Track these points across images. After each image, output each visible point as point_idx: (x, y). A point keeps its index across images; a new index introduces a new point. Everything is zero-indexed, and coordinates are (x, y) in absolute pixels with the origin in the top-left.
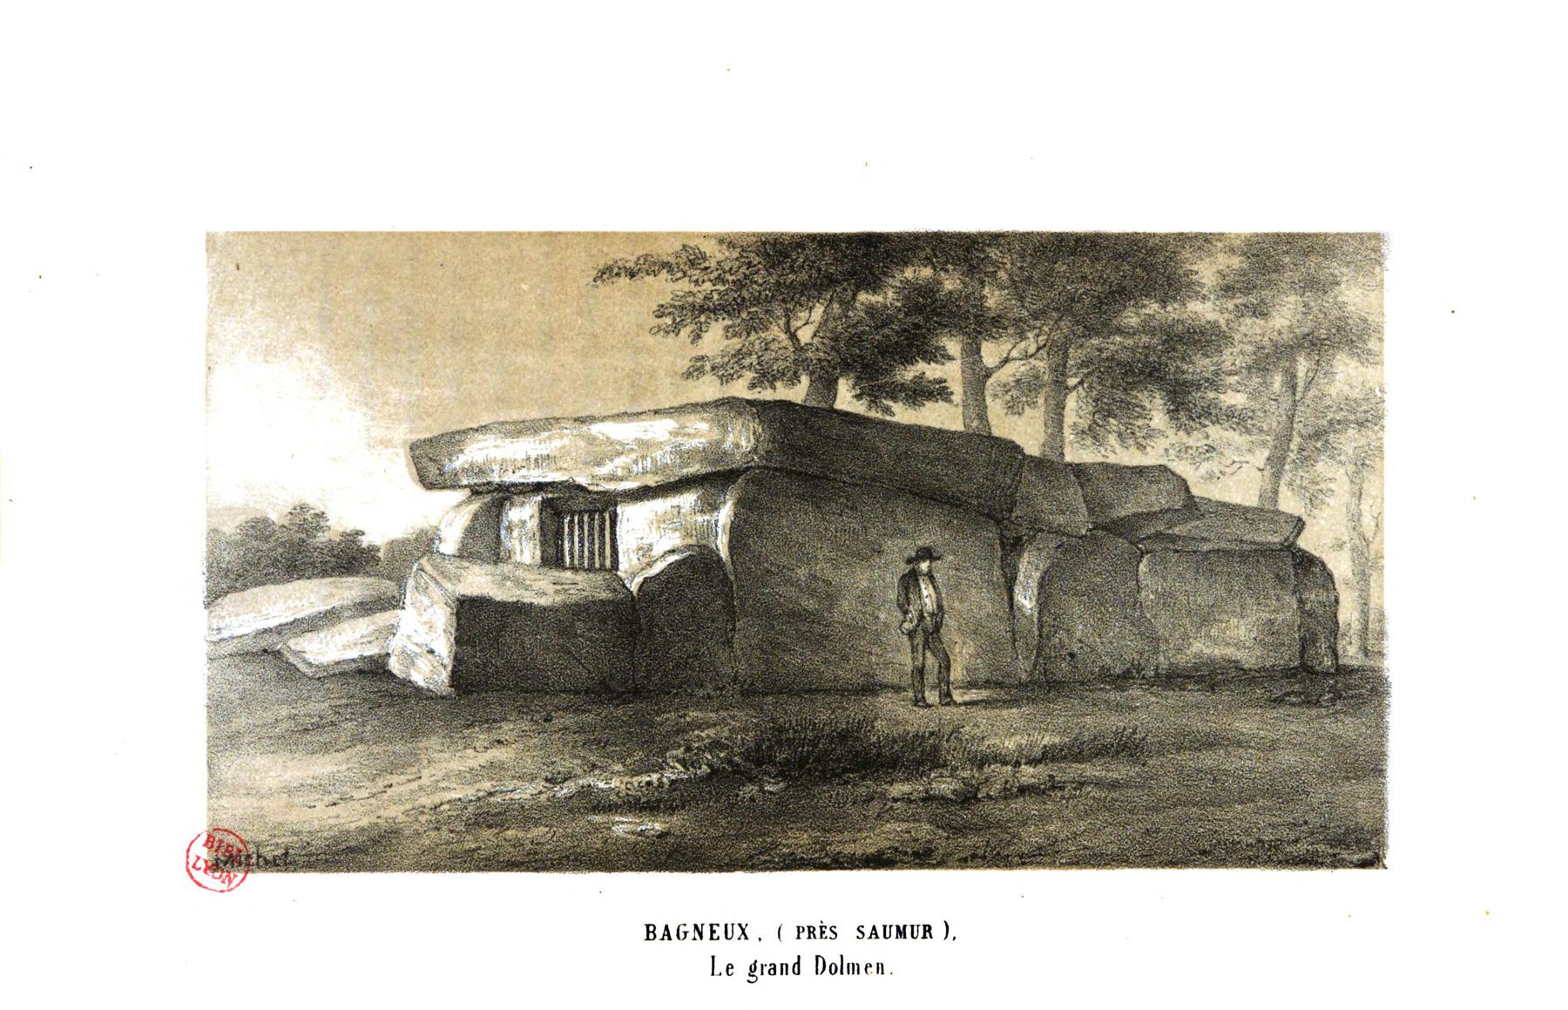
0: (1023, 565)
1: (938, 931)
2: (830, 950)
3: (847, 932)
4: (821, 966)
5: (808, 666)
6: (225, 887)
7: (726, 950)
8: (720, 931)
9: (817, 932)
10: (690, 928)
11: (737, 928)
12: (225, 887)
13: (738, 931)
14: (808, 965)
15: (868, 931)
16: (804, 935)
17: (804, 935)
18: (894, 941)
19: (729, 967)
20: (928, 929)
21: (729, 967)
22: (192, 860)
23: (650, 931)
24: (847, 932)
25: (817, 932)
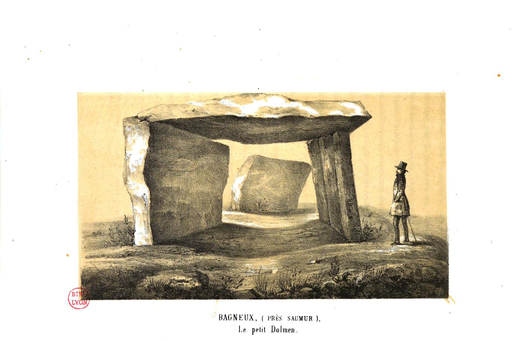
0: (238, 195)
1: (314, 318)
2: (277, 324)
3: (285, 318)
4: (274, 330)
5: (324, 122)
6: (86, 305)
7: (244, 324)
8: (243, 317)
9: (275, 318)
10: (233, 316)
11: (249, 316)
12: (86, 305)
13: (249, 317)
14: (269, 329)
15: (291, 318)
16: (271, 319)
17: (271, 319)
18: (299, 322)
19: (244, 330)
20: (311, 318)
21: (244, 330)
22: (71, 303)
23: (220, 317)
24: (285, 318)
25: (275, 318)
